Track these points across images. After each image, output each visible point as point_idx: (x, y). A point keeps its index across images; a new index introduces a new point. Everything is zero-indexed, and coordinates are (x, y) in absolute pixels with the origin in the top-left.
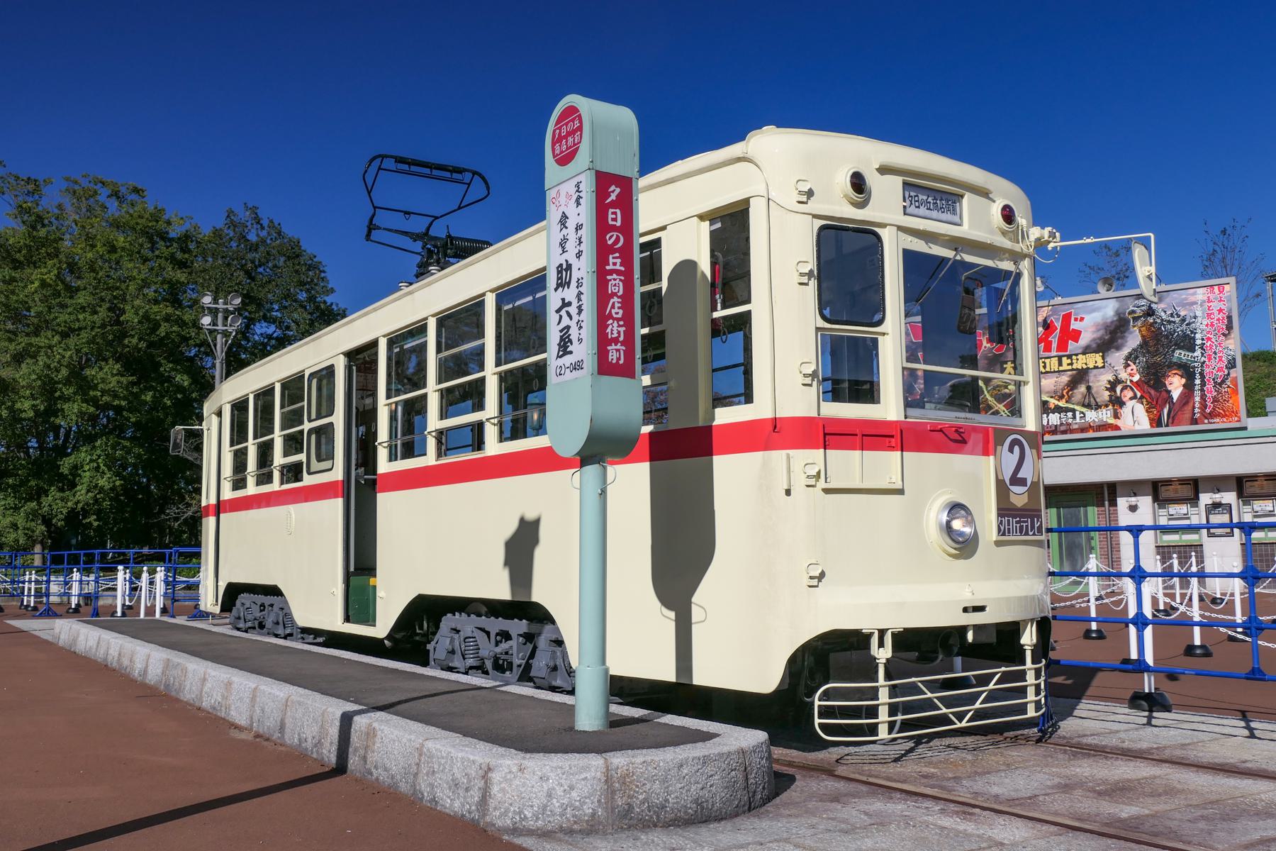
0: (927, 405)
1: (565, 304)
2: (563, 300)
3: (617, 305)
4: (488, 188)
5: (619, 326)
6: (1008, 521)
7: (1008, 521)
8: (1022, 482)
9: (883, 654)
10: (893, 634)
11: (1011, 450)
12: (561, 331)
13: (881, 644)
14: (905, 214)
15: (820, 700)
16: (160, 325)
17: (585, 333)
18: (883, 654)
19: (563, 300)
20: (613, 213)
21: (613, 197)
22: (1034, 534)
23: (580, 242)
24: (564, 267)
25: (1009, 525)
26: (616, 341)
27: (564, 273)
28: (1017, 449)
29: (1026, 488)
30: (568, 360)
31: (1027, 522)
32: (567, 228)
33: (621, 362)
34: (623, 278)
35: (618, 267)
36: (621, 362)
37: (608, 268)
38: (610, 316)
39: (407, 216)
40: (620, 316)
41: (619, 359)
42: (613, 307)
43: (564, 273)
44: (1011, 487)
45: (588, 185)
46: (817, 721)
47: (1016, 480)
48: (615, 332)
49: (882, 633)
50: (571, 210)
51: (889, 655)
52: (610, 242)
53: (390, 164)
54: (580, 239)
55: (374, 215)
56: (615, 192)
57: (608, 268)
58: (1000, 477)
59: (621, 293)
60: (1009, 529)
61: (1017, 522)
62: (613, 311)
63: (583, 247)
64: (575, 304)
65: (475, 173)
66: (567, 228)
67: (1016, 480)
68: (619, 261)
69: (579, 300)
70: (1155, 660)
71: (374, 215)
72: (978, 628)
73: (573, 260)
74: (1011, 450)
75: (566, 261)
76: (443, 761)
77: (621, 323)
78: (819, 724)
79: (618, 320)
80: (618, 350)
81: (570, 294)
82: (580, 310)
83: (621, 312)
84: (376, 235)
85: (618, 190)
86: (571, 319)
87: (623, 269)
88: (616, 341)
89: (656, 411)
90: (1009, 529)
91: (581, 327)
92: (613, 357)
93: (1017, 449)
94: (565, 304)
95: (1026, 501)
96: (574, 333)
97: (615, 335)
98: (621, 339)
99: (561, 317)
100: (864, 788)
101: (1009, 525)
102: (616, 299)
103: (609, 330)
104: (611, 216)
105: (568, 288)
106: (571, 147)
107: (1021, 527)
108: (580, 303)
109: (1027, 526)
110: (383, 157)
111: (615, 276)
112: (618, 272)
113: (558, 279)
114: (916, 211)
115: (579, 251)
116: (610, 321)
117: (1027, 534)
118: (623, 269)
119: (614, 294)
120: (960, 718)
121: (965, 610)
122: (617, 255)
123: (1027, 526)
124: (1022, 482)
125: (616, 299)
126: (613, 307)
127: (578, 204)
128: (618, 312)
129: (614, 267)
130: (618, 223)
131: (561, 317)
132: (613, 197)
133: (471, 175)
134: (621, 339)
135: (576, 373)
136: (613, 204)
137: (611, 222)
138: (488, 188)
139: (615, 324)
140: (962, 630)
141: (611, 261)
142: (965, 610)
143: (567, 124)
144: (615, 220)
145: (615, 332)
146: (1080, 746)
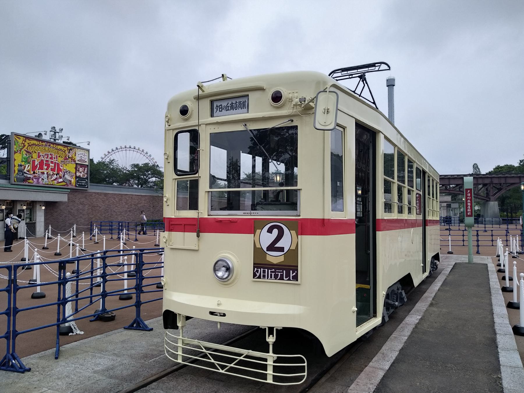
0: (387, 212)
6: (264, 272)
7: (264, 272)
9: (271, 340)
16: (51, 235)
18: (271, 340)
21: (469, 192)
26: (469, 212)
28: (275, 232)
35: (469, 202)
46: (306, 364)
47: (272, 247)
51: (274, 340)
56: (469, 191)
58: (258, 246)
63: (255, 213)
74: (270, 231)
78: (304, 363)
88: (469, 212)
89: (136, 234)
93: (275, 232)
119: (469, 206)
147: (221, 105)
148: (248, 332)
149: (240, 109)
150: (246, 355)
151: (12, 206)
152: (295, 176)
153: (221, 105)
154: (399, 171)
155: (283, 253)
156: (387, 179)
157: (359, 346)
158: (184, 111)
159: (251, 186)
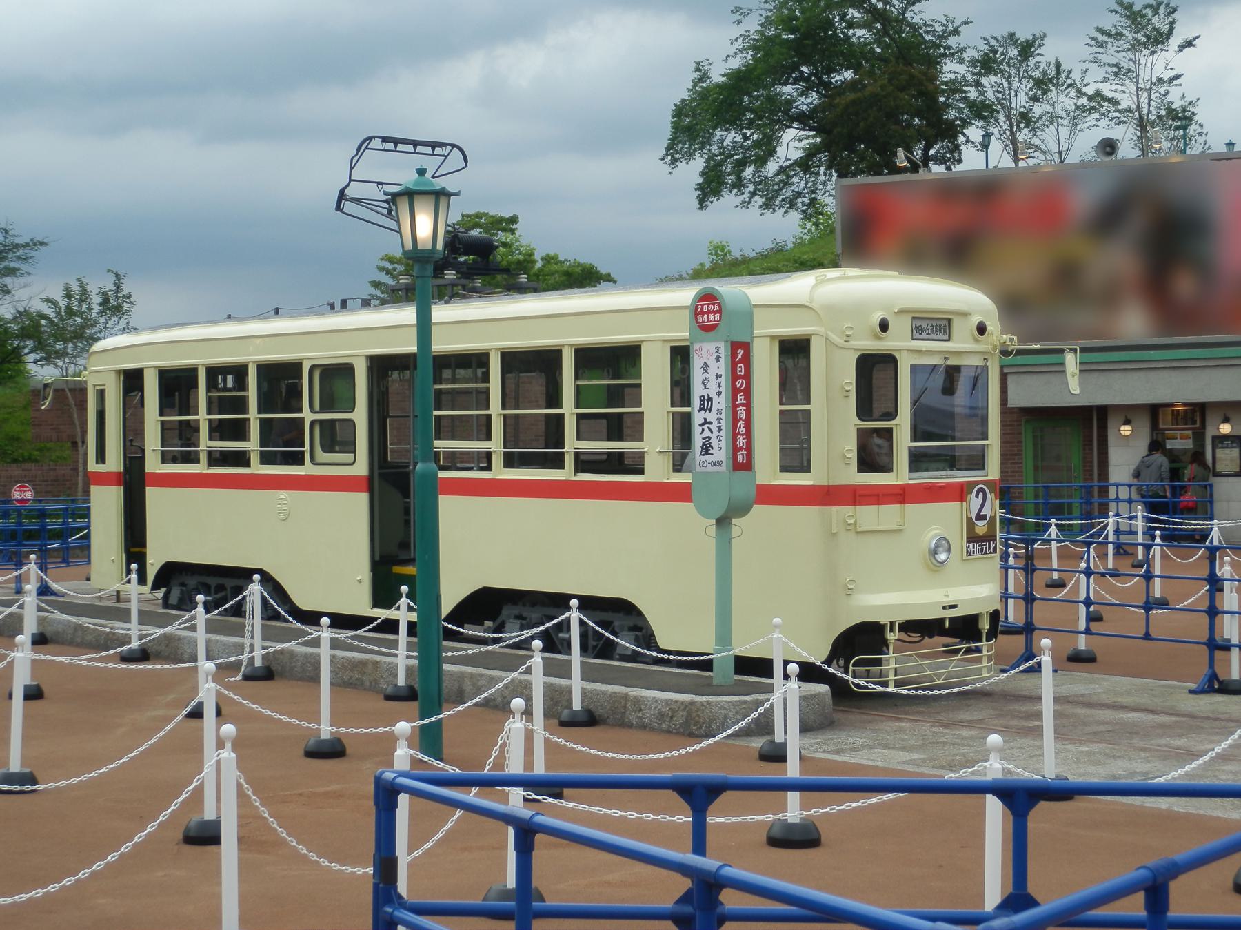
1: (706, 422)
2: (705, 419)
3: (742, 426)
4: (466, 160)
5: (743, 439)
6: (974, 545)
7: (974, 545)
8: (984, 518)
10: (899, 624)
11: (977, 496)
12: (703, 439)
13: (891, 630)
14: (913, 339)
15: (853, 666)
17: (723, 444)
19: (705, 419)
20: (740, 367)
21: (740, 356)
22: (991, 553)
23: (720, 386)
24: (706, 398)
25: (974, 548)
26: (741, 448)
27: (706, 402)
28: (981, 494)
29: (986, 521)
30: (708, 458)
31: (986, 545)
32: (708, 373)
33: (745, 461)
34: (745, 408)
36: (745, 461)
37: (737, 403)
38: (739, 434)
39: (380, 187)
40: (743, 432)
41: (743, 460)
42: (740, 427)
43: (706, 402)
44: (977, 522)
45: (724, 351)
47: (980, 517)
48: (741, 443)
49: (892, 623)
50: (712, 362)
52: (738, 386)
53: (376, 143)
54: (719, 384)
55: (347, 186)
56: (741, 352)
57: (737, 403)
58: (969, 516)
59: (744, 418)
60: (974, 551)
61: (979, 546)
62: (740, 430)
64: (715, 424)
65: (453, 146)
66: (708, 373)
67: (980, 517)
68: (743, 397)
69: (719, 422)
70: (408, 891)
71: (347, 186)
72: (951, 619)
73: (713, 395)
74: (977, 496)
75: (708, 395)
76: (649, 703)
77: (744, 437)
79: (743, 435)
80: (743, 454)
81: (711, 417)
82: (720, 429)
83: (744, 430)
84: (348, 206)
85: (742, 351)
86: (712, 432)
87: (745, 402)
88: (741, 448)
90: (974, 551)
91: (720, 440)
92: (740, 459)
93: (981, 494)
94: (706, 422)
95: (986, 530)
96: (714, 442)
97: (741, 445)
98: (745, 447)
99: (703, 430)
100: (884, 718)
101: (974, 548)
102: (742, 422)
103: (738, 442)
104: (739, 369)
105: (710, 412)
106: (711, 321)
107: (982, 549)
108: (720, 425)
109: (986, 548)
110: (370, 138)
111: (741, 407)
112: (742, 405)
113: (701, 405)
114: (921, 337)
115: (719, 392)
116: (739, 437)
117: (986, 553)
118: (745, 402)
119: (741, 419)
120: (939, 677)
121: (944, 608)
122: (742, 394)
123: (986, 548)
124: (984, 518)
125: (742, 422)
126: (740, 427)
127: (718, 361)
128: (742, 430)
129: (741, 402)
130: (743, 373)
131: (703, 430)
132: (740, 356)
133: (450, 148)
134: (745, 447)
135: (716, 469)
136: (740, 362)
137: (739, 373)
138: (466, 160)
139: (741, 438)
140: (942, 621)
141: (739, 398)
142: (944, 608)
143: (708, 305)
144: (740, 371)
145: (741, 443)
146: (1018, 696)
147: (921, 326)
148: (1142, 367)
149: (758, 200)
150: (959, 653)
151: (1198, 425)
152: (25, 339)
153: (921, 326)
154: (1099, 445)
155: (986, 521)
156: (585, 344)
157: (985, 728)
158: (884, 326)
159: (458, 455)
